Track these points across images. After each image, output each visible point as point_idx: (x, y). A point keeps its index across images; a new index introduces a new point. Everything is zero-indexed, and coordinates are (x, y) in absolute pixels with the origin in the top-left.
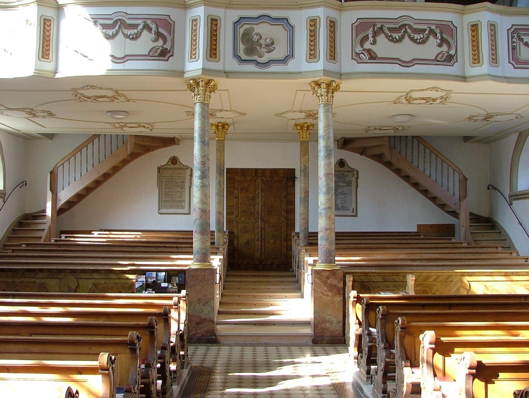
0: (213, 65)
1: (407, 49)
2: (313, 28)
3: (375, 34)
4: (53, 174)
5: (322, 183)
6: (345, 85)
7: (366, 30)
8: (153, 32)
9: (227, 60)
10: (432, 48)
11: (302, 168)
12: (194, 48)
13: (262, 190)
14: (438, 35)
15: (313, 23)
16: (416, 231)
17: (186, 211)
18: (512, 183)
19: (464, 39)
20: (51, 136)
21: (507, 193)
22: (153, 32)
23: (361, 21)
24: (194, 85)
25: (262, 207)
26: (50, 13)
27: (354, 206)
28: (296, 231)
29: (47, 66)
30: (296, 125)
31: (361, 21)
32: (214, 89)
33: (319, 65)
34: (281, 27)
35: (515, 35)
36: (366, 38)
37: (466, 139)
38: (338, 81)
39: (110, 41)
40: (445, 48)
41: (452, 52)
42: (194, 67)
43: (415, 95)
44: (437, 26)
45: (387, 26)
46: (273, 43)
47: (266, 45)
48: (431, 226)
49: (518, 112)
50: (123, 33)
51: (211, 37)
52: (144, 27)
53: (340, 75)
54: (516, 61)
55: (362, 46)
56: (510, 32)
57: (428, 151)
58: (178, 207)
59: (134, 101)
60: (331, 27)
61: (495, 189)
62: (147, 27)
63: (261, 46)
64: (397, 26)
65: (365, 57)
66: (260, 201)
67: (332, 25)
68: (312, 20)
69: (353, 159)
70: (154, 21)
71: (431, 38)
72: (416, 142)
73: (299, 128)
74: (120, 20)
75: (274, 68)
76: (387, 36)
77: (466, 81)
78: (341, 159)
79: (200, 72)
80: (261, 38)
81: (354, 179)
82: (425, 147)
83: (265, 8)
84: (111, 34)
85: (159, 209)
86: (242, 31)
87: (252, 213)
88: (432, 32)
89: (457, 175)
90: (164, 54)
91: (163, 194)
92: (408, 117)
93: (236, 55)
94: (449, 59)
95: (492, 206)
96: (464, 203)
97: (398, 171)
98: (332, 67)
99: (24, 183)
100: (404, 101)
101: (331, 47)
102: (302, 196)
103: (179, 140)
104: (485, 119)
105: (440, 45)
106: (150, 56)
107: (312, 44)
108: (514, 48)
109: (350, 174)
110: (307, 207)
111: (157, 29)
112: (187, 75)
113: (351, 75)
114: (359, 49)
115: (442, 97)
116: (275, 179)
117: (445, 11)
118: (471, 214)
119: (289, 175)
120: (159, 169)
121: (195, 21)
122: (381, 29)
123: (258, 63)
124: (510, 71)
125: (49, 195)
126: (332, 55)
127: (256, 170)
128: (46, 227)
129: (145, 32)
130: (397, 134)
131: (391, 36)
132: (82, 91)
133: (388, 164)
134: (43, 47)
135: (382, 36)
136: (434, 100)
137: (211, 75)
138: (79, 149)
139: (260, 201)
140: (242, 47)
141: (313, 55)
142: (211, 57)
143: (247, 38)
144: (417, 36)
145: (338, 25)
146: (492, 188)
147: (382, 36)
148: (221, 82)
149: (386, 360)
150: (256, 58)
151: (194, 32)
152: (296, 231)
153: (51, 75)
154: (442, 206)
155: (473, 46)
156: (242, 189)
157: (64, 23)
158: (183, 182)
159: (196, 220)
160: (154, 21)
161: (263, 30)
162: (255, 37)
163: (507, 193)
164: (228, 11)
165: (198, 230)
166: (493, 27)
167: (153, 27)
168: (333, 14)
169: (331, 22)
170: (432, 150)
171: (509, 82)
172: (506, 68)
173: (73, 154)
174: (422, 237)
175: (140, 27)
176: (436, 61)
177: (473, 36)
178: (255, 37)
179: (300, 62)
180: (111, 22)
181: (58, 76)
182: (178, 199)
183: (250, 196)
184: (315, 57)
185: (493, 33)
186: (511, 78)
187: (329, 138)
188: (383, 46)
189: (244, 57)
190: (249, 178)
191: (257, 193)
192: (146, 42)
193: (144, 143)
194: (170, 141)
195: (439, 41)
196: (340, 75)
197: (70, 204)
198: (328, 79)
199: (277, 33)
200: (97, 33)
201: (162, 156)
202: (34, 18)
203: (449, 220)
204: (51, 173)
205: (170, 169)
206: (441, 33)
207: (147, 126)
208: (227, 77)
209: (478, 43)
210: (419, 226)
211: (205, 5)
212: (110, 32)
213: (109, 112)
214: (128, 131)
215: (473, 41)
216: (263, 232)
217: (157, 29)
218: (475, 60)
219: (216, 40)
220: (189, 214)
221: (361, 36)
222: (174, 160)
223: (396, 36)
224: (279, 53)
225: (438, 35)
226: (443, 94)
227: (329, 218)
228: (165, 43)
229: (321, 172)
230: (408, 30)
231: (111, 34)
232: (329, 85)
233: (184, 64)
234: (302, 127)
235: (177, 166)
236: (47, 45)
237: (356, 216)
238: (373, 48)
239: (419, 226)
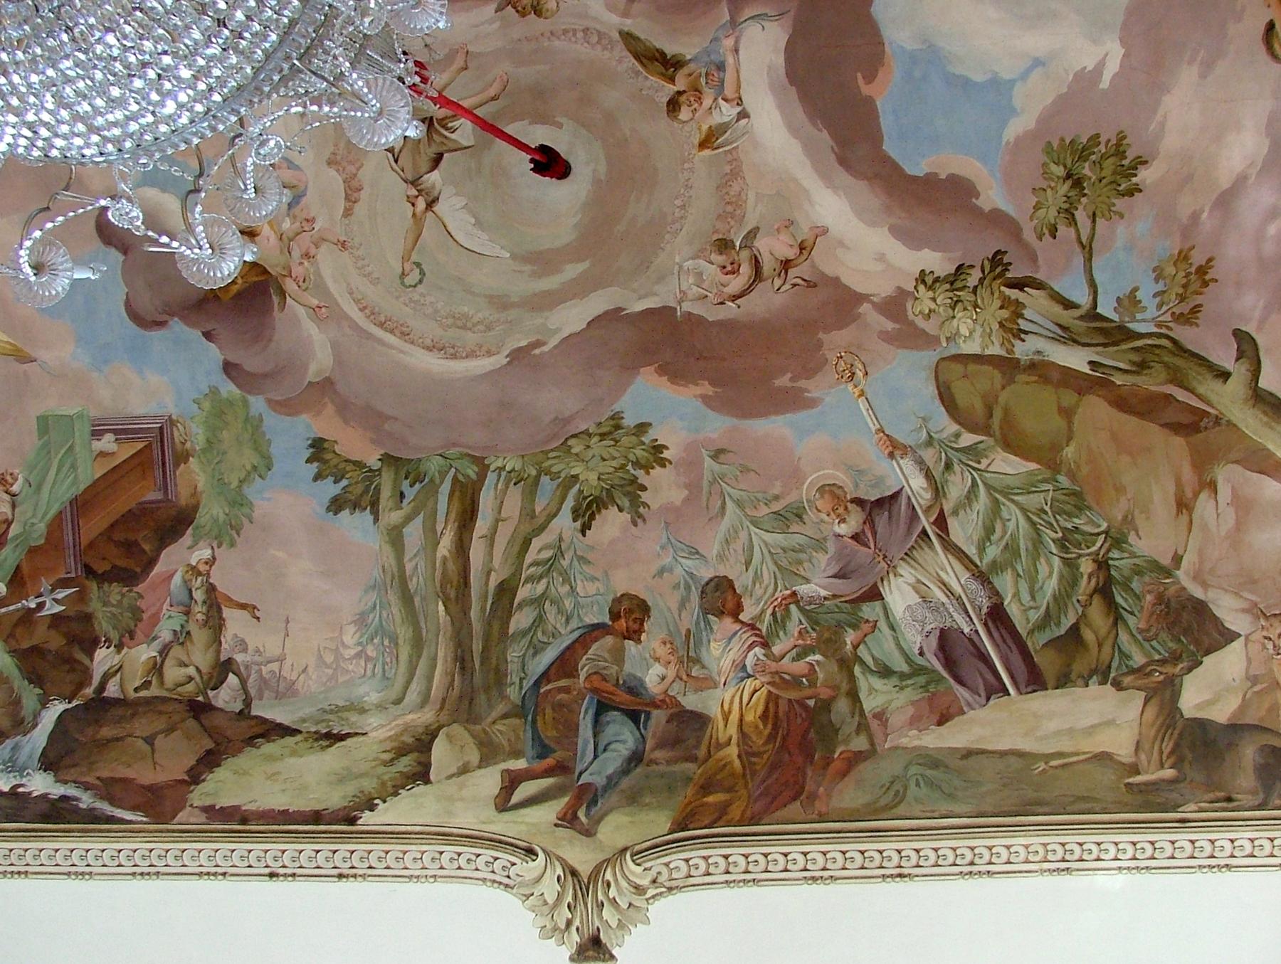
222: (875, 716)
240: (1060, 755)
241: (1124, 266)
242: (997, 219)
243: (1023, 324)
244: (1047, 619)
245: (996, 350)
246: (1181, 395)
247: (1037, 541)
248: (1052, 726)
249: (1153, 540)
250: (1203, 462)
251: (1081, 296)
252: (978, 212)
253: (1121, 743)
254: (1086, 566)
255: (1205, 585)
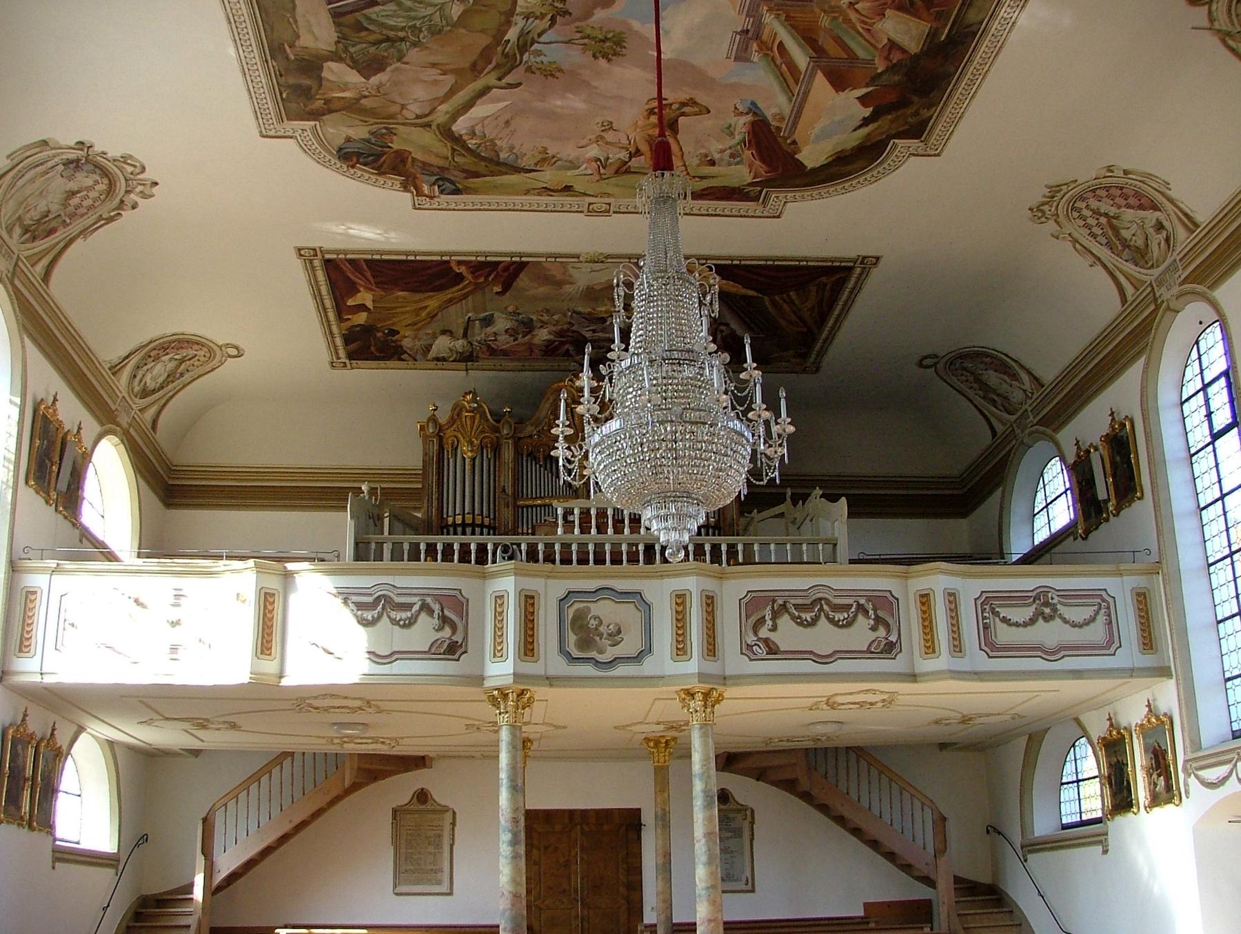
0: (530, 668)
1: (824, 636)
2: (680, 609)
3: (775, 615)
4: (207, 823)
5: (700, 847)
6: (730, 692)
7: (759, 609)
8: (436, 615)
9: (550, 660)
10: (861, 633)
11: (659, 813)
12: (499, 640)
13: (583, 849)
14: (871, 612)
15: (681, 599)
16: (862, 914)
17: (444, 888)
18: (1025, 826)
19: (910, 616)
20: (196, 753)
21: (1018, 841)
22: (436, 615)
23: (754, 594)
24: (498, 697)
25: (582, 879)
26: (274, 583)
27: (748, 873)
28: (647, 920)
29: (270, 666)
30: (647, 740)
31: (754, 594)
32: (528, 704)
33: (692, 666)
34: (632, 606)
35: (987, 607)
36: (761, 621)
37: (943, 746)
38: (720, 688)
39: (369, 629)
40: (882, 632)
41: (893, 638)
42: (500, 671)
43: (840, 699)
44: (869, 599)
45: (793, 601)
46: (619, 632)
47: (610, 635)
48: (890, 905)
49: (1013, 712)
50: (389, 617)
51: (526, 623)
52: (421, 609)
53: (724, 679)
54: (991, 647)
55: (756, 633)
56: (979, 602)
57: (874, 772)
58: (429, 882)
59: (389, 712)
60: (708, 605)
61: (999, 833)
62: (425, 607)
63: (601, 635)
64: (808, 602)
65: (761, 651)
66: (578, 868)
67: (710, 602)
68: (678, 596)
69: (745, 789)
70: (437, 598)
71: (860, 617)
72: (853, 756)
73: (652, 744)
74: (384, 596)
75: (622, 670)
76: (793, 618)
77: (916, 681)
78: (722, 790)
79: (510, 680)
80: (601, 623)
81: (746, 825)
82: (869, 764)
83: (606, 577)
84: (370, 618)
85: (395, 886)
86: (571, 612)
87: (564, 891)
88: (861, 608)
89: (928, 811)
90: (453, 650)
91: (403, 858)
92: (834, 725)
93: (563, 651)
94: (889, 649)
95: (996, 865)
96: (942, 861)
97: (824, 808)
98: (712, 667)
99: (144, 838)
100: (825, 707)
101: (709, 643)
102: (661, 861)
103: (432, 759)
104: (963, 722)
105: (874, 629)
106: (431, 653)
107: (680, 632)
108: (986, 627)
109: (740, 816)
110: (668, 879)
111: (442, 610)
112: (488, 684)
113: (739, 679)
114: (751, 638)
115: (884, 701)
116: (606, 827)
117: (879, 576)
118: (957, 880)
119: (630, 821)
120: (395, 811)
121: (500, 598)
122: (784, 606)
123: (597, 663)
124: (982, 662)
125: (200, 861)
126: (711, 648)
127: (571, 813)
128: (192, 921)
129: (423, 616)
130: (819, 745)
131: (800, 617)
132: (311, 701)
133: (806, 797)
134: (263, 637)
135: (786, 617)
136: (871, 704)
137: (528, 684)
138: (256, 777)
139: (578, 868)
140: (572, 638)
141: (681, 649)
142: (526, 654)
143: (579, 622)
144: (839, 616)
145: (718, 601)
146: (994, 830)
147: (786, 617)
148: (540, 692)
149: (741, 560)
150: (594, 654)
151: (499, 615)
152: (647, 920)
153: (273, 681)
154: (907, 868)
155: (925, 627)
156: (546, 848)
157: (293, 599)
158: (440, 836)
159: (504, 911)
160: (437, 598)
161: (604, 610)
162: (592, 621)
163: (1018, 841)
164: (550, 581)
165: (509, 926)
166: (952, 598)
167: (436, 607)
168: (710, 585)
169: (708, 597)
170: (883, 770)
171: (982, 680)
172: (976, 658)
173: (245, 786)
174: (872, 925)
175: (416, 608)
176: (869, 653)
177: (924, 612)
178: (592, 621)
179: (662, 661)
180: (370, 599)
181: (285, 682)
182: (429, 867)
183: (562, 860)
184: (685, 653)
185: (953, 606)
186: (984, 673)
187: (709, 777)
188: (787, 634)
189: (576, 653)
190: (558, 827)
191: (573, 853)
192: (425, 632)
193: (373, 767)
194: (419, 762)
195: (872, 622)
196: (724, 679)
197: (233, 877)
198: (706, 687)
199: (625, 614)
200: (345, 617)
201: (401, 788)
202: (251, 594)
203: (920, 892)
204: (205, 820)
205: (418, 811)
206: (875, 610)
207: (388, 741)
208: (551, 685)
209: (931, 622)
210: (866, 905)
211: (516, 574)
212: (369, 615)
213: (335, 724)
214: (350, 748)
215: (924, 620)
216: (586, 925)
217: (442, 610)
218: (928, 648)
219: (533, 629)
220: (451, 894)
221: (753, 619)
222: (422, 796)
223: (807, 616)
224: (630, 645)
225: (871, 612)
226: (885, 697)
227: (713, 903)
228: (454, 633)
229: (699, 830)
230: (825, 607)
231: (370, 618)
232: (706, 695)
233: (483, 666)
234: (657, 743)
235: (428, 806)
236: (269, 633)
237: (753, 891)
238: (773, 636)
239: (866, 905)
240: (296, 22)
241: (554, 49)
242: (588, 14)
243: (530, 20)
244: (368, 18)
245: (518, 10)
246: (490, 67)
247: (414, 19)
248: (312, 19)
249: (414, 55)
250: (458, 72)
251: (542, 39)
252: (595, 8)
253: (306, 41)
254: (401, 34)
255: (393, 71)
